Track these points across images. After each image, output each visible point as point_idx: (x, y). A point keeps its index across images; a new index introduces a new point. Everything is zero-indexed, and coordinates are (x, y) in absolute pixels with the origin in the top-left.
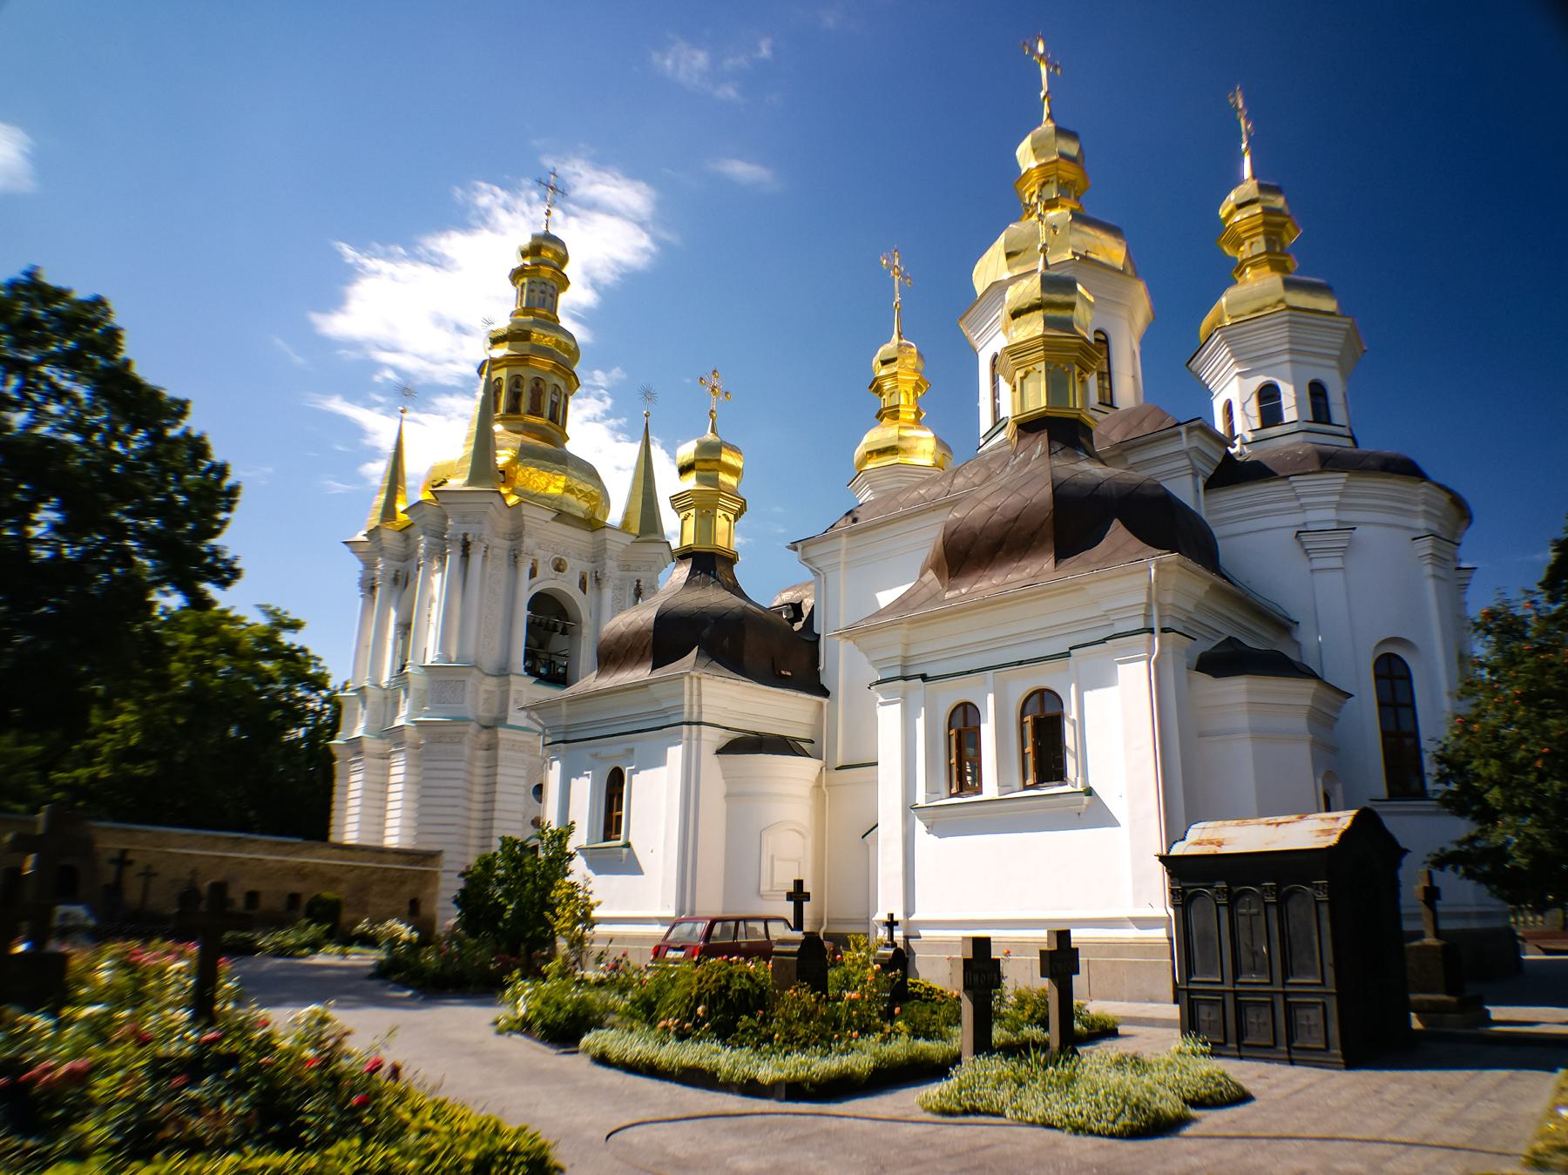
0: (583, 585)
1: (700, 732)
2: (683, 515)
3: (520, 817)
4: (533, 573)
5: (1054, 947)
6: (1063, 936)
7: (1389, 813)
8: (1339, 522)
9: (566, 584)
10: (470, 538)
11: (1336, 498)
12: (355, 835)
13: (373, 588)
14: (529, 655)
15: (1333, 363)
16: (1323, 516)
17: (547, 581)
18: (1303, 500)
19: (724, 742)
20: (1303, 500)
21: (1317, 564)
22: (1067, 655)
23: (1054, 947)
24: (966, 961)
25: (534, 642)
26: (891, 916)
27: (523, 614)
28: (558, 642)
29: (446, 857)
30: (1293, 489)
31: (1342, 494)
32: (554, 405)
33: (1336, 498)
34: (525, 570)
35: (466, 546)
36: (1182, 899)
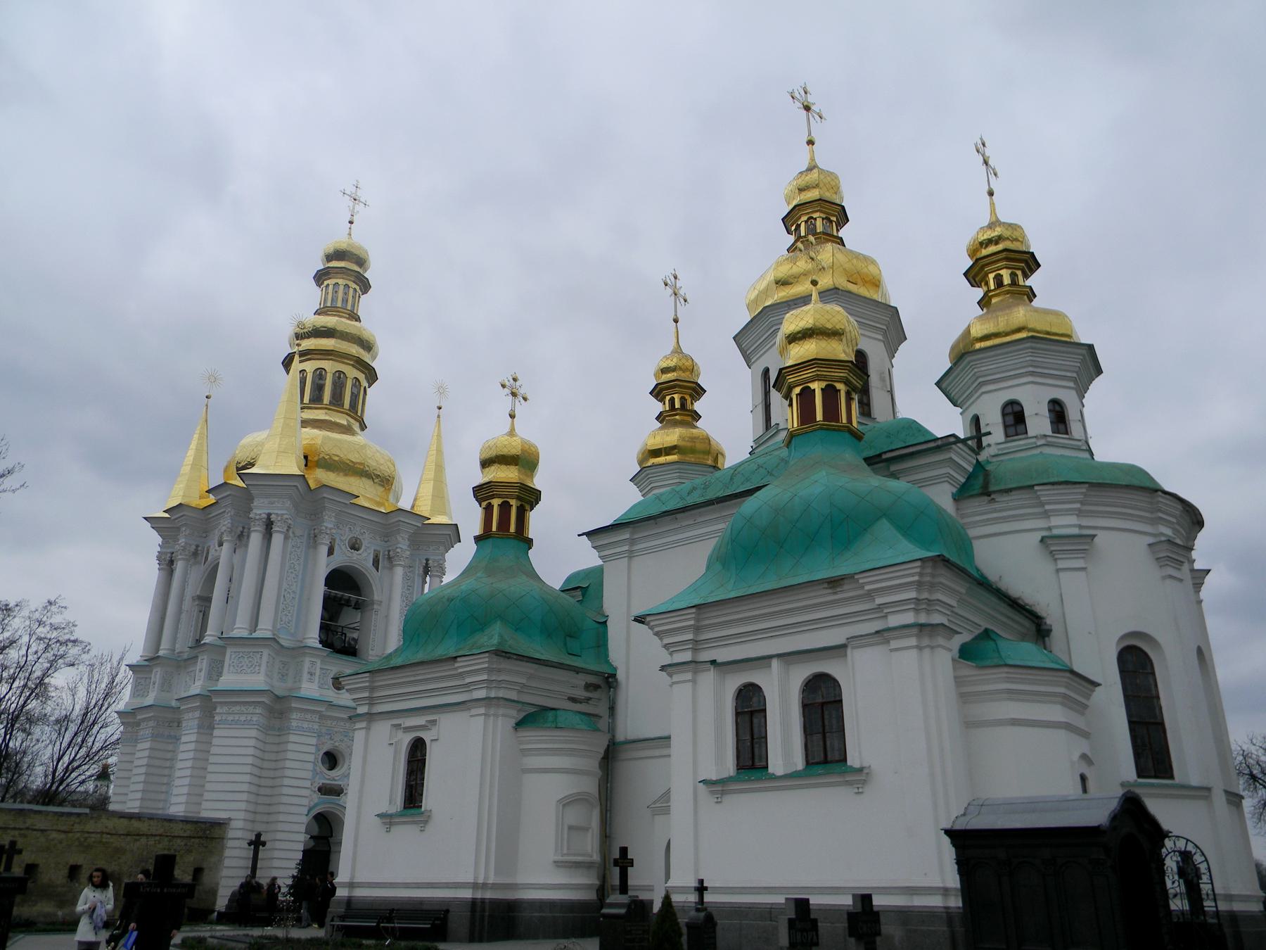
0: (376, 563)
1: (556, 717)
2: (484, 504)
3: (308, 784)
4: (331, 552)
5: (859, 909)
6: (866, 899)
7: (1151, 796)
8: (1080, 527)
9: (362, 560)
10: (273, 517)
11: (1078, 506)
12: (137, 804)
13: (171, 562)
14: (324, 628)
15: (1072, 384)
16: (1065, 523)
17: (343, 558)
18: (1047, 507)
19: (522, 715)
20: (1047, 507)
21: (1061, 564)
22: (844, 646)
23: (859, 909)
24: (790, 920)
25: (326, 616)
26: (701, 881)
27: (319, 589)
28: (349, 618)
29: (234, 824)
30: (1038, 497)
31: (1082, 503)
32: (354, 398)
33: (1078, 506)
34: (324, 550)
35: (269, 525)
36: (963, 865)
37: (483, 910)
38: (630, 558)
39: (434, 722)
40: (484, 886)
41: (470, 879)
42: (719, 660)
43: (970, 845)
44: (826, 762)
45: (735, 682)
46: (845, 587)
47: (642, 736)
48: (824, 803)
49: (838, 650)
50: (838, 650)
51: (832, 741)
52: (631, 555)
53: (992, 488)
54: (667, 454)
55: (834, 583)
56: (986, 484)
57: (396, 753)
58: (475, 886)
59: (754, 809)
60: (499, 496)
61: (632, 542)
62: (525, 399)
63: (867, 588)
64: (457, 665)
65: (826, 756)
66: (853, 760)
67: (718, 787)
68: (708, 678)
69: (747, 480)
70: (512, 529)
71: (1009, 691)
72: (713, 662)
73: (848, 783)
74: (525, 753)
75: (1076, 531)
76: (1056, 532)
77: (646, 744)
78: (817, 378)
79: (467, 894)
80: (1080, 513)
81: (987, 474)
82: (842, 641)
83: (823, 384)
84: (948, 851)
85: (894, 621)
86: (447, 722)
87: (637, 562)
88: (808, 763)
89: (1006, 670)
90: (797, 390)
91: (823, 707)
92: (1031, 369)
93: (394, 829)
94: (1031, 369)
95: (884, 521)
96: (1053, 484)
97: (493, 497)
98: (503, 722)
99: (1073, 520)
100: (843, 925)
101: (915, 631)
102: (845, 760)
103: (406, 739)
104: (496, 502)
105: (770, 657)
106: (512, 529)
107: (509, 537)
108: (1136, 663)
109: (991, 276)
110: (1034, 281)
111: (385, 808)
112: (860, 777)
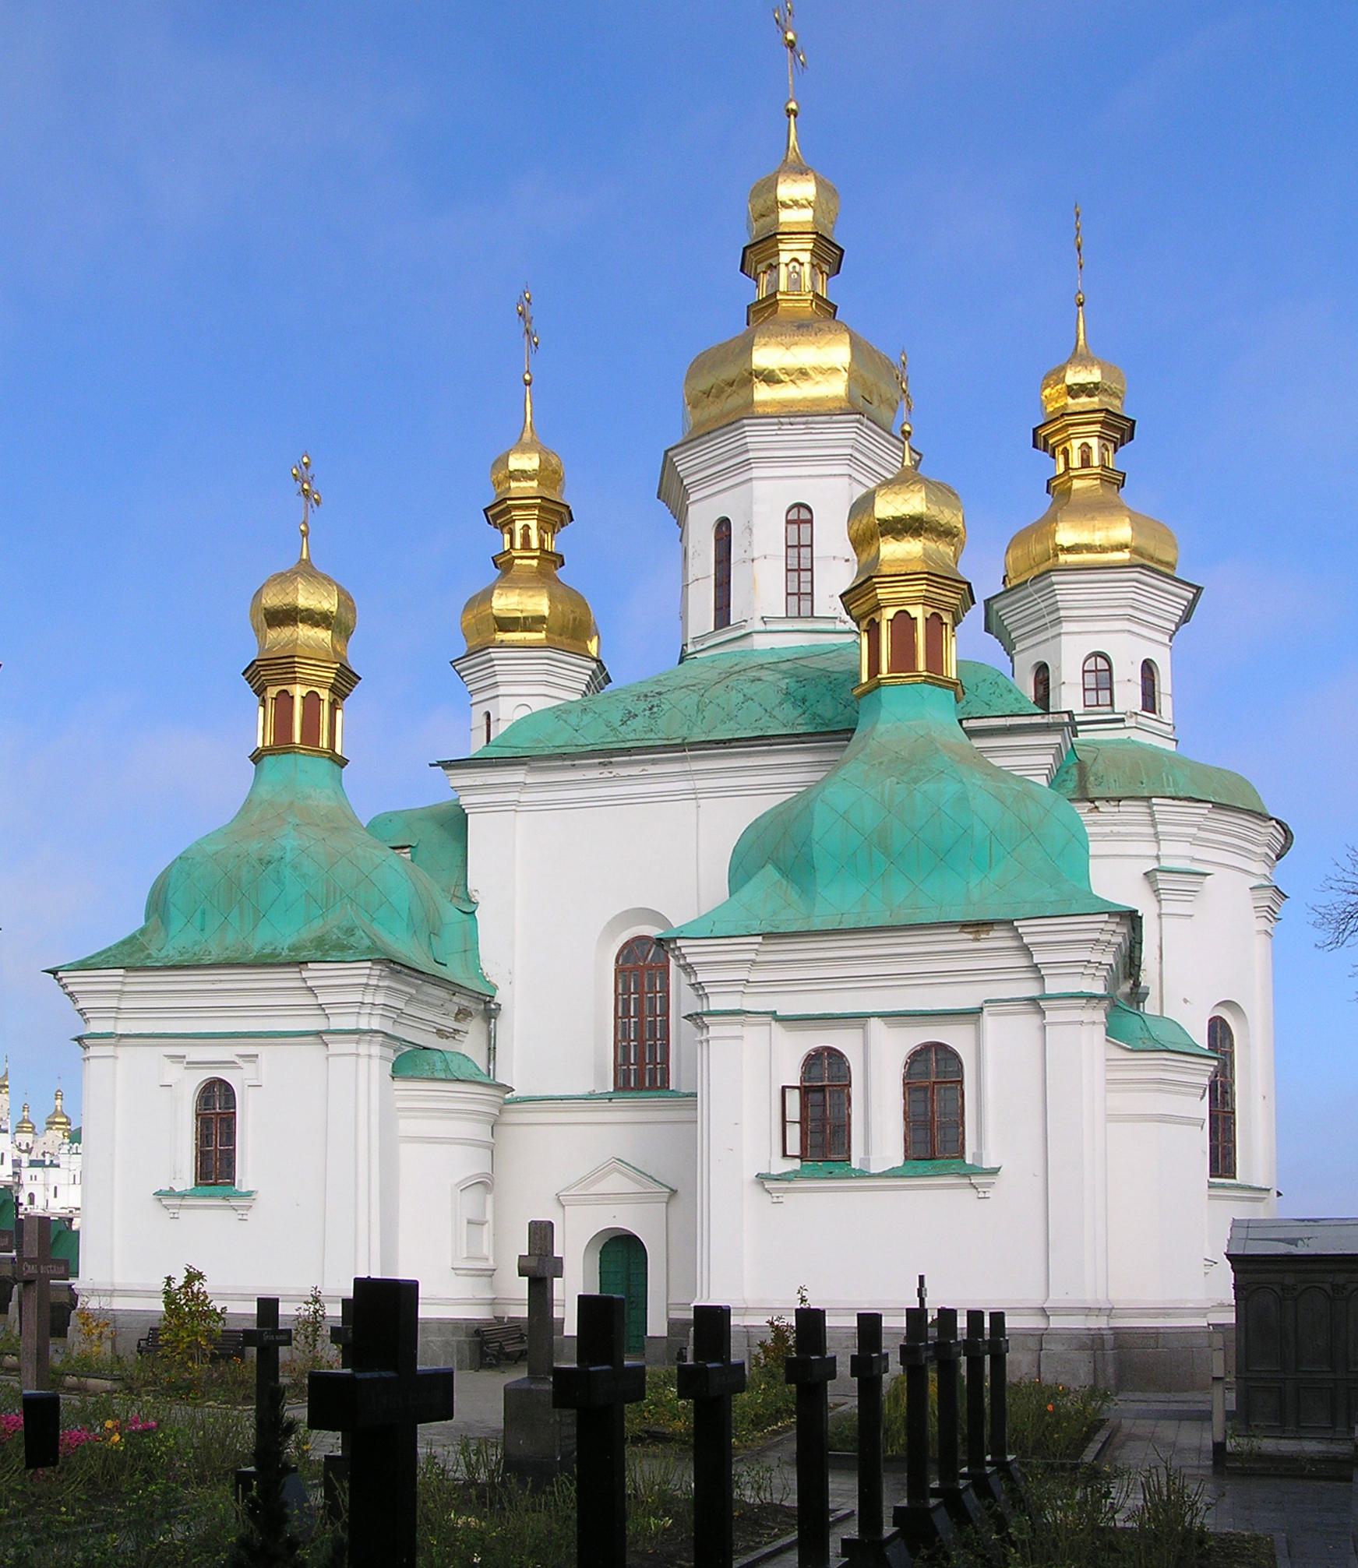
11: (1194, 830)
16: (1176, 853)
36: (1240, 1288)
37: (867, 1364)
43: (1247, 1267)
45: (799, 1045)
46: (992, 934)
48: (936, 1201)
53: (1093, 793)
56: (1082, 786)
59: (823, 1205)
60: (305, 682)
62: (317, 502)
64: (305, 974)
69: (730, 717)
70: (324, 743)
76: (1166, 863)
80: (1194, 841)
81: (1081, 766)
84: (1226, 1276)
90: (889, 613)
92: (1130, 611)
94: (1130, 611)
97: (294, 681)
98: (374, 1062)
99: (1183, 849)
103: (189, 1086)
108: (1219, 1031)
109: (1076, 443)
112: (979, 1175)
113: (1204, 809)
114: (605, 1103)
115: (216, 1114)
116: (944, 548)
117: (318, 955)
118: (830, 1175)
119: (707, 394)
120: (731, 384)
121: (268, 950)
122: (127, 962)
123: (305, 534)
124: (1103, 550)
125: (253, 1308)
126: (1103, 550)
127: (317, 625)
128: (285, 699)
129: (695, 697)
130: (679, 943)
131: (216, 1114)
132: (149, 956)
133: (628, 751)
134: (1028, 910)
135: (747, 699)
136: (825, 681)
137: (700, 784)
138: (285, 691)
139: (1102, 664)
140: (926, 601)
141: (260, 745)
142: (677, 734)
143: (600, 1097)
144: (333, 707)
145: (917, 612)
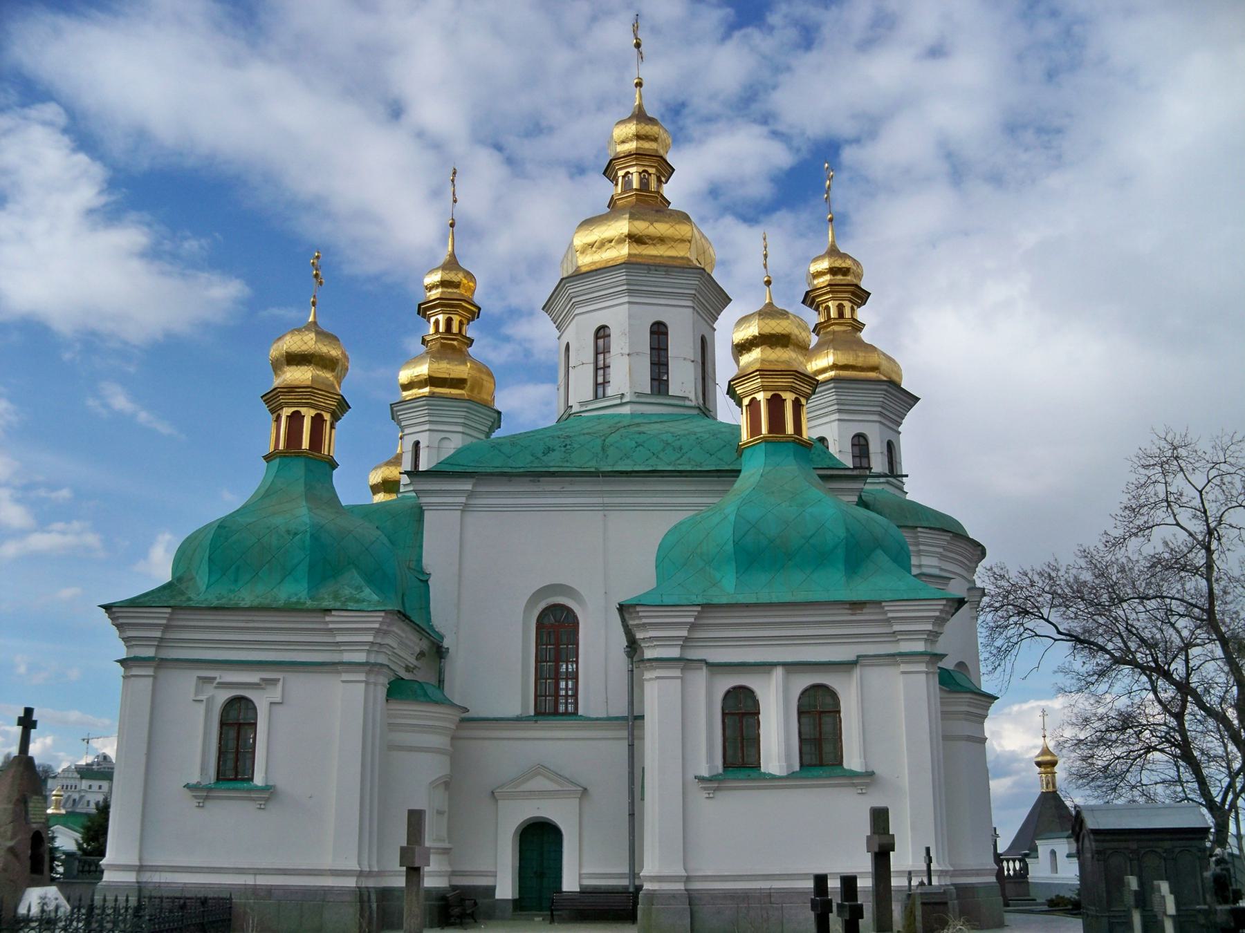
8: (941, 569)
18: (922, 547)
20: (922, 547)
38: (463, 511)
39: (274, 682)
40: (370, 874)
41: (353, 865)
42: (711, 660)
44: (821, 765)
46: (865, 611)
47: (491, 716)
49: (847, 666)
50: (847, 666)
51: (828, 748)
52: (465, 508)
54: (451, 387)
55: (856, 606)
57: (208, 711)
58: (360, 874)
59: (739, 807)
61: (471, 495)
63: (890, 615)
64: (328, 619)
65: (821, 759)
66: (853, 760)
67: (712, 783)
68: (700, 678)
70: (305, 444)
71: (968, 713)
72: (704, 661)
73: (854, 785)
74: (392, 727)
75: (936, 572)
76: (925, 570)
77: (486, 724)
78: (792, 389)
79: (351, 882)
80: (942, 557)
82: (852, 657)
83: (769, 394)
85: (905, 647)
86: (298, 684)
87: (470, 518)
88: (802, 765)
89: (969, 696)
91: (819, 719)
93: (209, 804)
95: (879, 552)
96: (931, 528)
99: (934, 561)
100: (511, 906)
101: (927, 658)
102: (841, 763)
104: (308, 414)
105: (774, 665)
106: (305, 444)
107: (300, 455)
110: (862, 314)
111: (195, 779)
113: (947, 537)
114: (532, 724)
115: (237, 723)
116: (328, 375)
117: (338, 605)
118: (749, 778)
119: (592, 245)
120: (611, 241)
121: (294, 599)
122: (172, 603)
123: (314, 304)
124: (862, 369)
125: (810, 884)
126: (862, 369)
127: (749, 350)
128: (296, 419)
129: (599, 441)
130: (638, 609)
131: (237, 723)
132: (189, 599)
133: (553, 474)
134: (889, 596)
135: (638, 445)
136: (693, 437)
137: (606, 500)
138: (298, 412)
139: (862, 441)
140: (764, 389)
141: (272, 449)
142: (591, 466)
143: (527, 719)
144: (332, 427)
145: (761, 396)
